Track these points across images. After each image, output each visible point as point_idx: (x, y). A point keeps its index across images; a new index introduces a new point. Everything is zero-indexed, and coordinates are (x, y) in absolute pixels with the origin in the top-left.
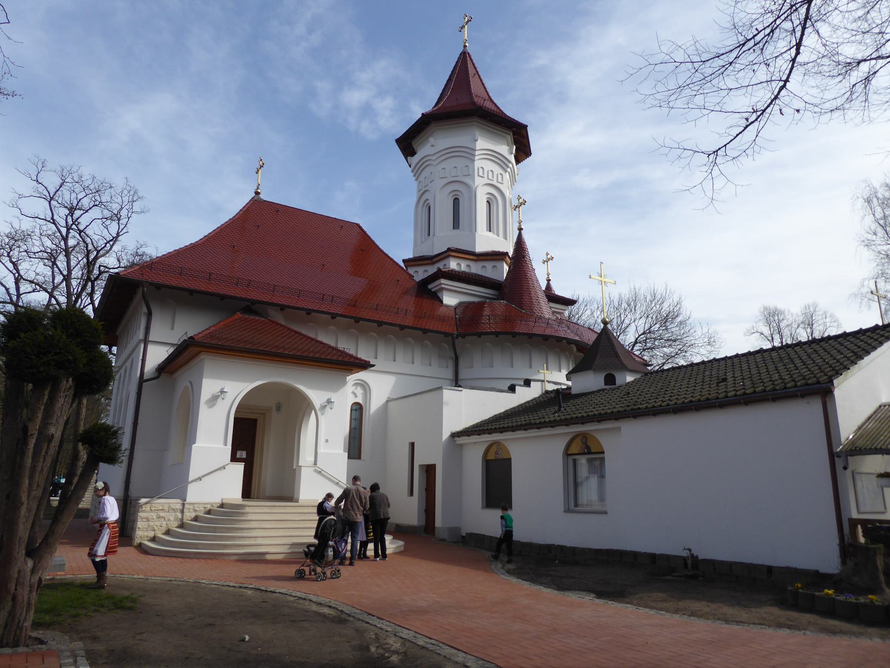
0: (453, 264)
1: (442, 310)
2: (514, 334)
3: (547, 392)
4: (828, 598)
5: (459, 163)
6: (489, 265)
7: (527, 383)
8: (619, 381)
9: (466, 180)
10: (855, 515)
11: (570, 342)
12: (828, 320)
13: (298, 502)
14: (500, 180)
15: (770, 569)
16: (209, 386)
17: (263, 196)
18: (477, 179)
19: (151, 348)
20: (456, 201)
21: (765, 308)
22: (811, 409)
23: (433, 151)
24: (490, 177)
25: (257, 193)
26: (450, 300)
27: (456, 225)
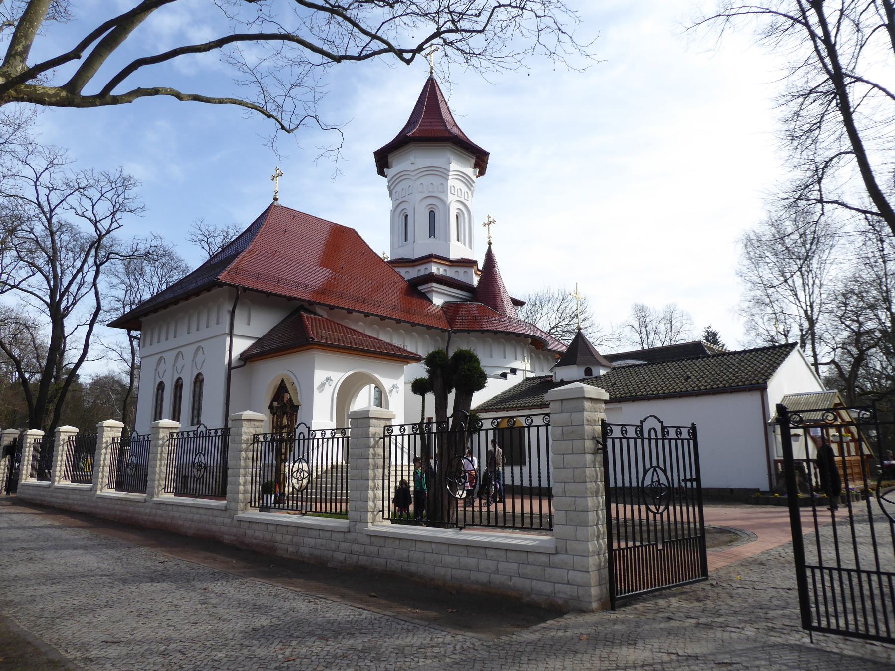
0: (434, 269)
1: (430, 309)
2: (483, 331)
3: (527, 379)
4: (776, 497)
5: (436, 181)
6: (461, 270)
7: (513, 371)
8: (595, 374)
9: (442, 196)
10: (776, 458)
11: (527, 336)
12: (685, 318)
14: (466, 198)
15: (732, 490)
16: (319, 375)
17: (282, 202)
18: (450, 196)
19: (235, 340)
20: (432, 214)
21: (636, 306)
22: (756, 397)
23: (413, 168)
24: (460, 195)
25: (276, 199)
26: (438, 301)
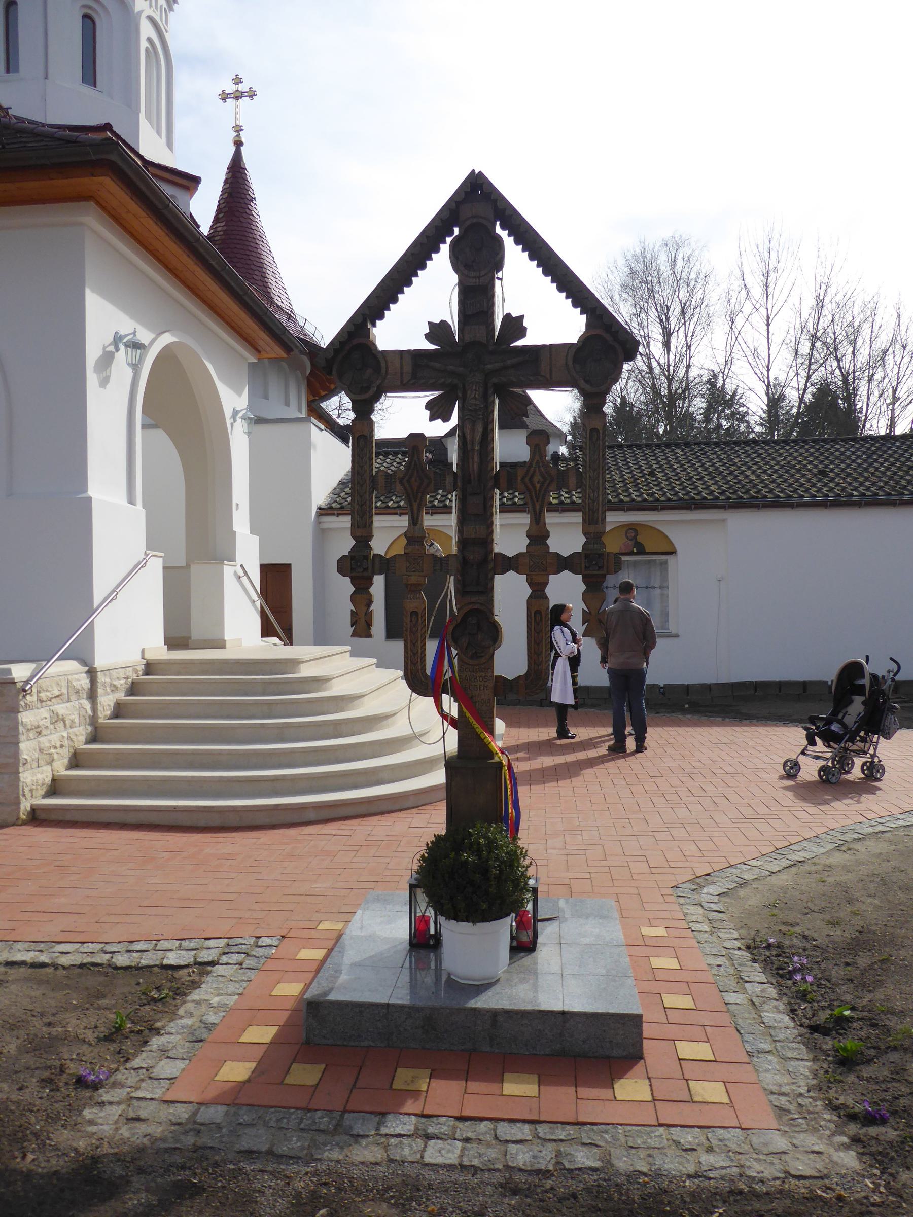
13: (224, 647)
27: (90, 76)
